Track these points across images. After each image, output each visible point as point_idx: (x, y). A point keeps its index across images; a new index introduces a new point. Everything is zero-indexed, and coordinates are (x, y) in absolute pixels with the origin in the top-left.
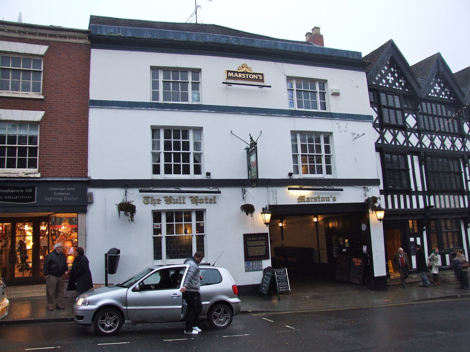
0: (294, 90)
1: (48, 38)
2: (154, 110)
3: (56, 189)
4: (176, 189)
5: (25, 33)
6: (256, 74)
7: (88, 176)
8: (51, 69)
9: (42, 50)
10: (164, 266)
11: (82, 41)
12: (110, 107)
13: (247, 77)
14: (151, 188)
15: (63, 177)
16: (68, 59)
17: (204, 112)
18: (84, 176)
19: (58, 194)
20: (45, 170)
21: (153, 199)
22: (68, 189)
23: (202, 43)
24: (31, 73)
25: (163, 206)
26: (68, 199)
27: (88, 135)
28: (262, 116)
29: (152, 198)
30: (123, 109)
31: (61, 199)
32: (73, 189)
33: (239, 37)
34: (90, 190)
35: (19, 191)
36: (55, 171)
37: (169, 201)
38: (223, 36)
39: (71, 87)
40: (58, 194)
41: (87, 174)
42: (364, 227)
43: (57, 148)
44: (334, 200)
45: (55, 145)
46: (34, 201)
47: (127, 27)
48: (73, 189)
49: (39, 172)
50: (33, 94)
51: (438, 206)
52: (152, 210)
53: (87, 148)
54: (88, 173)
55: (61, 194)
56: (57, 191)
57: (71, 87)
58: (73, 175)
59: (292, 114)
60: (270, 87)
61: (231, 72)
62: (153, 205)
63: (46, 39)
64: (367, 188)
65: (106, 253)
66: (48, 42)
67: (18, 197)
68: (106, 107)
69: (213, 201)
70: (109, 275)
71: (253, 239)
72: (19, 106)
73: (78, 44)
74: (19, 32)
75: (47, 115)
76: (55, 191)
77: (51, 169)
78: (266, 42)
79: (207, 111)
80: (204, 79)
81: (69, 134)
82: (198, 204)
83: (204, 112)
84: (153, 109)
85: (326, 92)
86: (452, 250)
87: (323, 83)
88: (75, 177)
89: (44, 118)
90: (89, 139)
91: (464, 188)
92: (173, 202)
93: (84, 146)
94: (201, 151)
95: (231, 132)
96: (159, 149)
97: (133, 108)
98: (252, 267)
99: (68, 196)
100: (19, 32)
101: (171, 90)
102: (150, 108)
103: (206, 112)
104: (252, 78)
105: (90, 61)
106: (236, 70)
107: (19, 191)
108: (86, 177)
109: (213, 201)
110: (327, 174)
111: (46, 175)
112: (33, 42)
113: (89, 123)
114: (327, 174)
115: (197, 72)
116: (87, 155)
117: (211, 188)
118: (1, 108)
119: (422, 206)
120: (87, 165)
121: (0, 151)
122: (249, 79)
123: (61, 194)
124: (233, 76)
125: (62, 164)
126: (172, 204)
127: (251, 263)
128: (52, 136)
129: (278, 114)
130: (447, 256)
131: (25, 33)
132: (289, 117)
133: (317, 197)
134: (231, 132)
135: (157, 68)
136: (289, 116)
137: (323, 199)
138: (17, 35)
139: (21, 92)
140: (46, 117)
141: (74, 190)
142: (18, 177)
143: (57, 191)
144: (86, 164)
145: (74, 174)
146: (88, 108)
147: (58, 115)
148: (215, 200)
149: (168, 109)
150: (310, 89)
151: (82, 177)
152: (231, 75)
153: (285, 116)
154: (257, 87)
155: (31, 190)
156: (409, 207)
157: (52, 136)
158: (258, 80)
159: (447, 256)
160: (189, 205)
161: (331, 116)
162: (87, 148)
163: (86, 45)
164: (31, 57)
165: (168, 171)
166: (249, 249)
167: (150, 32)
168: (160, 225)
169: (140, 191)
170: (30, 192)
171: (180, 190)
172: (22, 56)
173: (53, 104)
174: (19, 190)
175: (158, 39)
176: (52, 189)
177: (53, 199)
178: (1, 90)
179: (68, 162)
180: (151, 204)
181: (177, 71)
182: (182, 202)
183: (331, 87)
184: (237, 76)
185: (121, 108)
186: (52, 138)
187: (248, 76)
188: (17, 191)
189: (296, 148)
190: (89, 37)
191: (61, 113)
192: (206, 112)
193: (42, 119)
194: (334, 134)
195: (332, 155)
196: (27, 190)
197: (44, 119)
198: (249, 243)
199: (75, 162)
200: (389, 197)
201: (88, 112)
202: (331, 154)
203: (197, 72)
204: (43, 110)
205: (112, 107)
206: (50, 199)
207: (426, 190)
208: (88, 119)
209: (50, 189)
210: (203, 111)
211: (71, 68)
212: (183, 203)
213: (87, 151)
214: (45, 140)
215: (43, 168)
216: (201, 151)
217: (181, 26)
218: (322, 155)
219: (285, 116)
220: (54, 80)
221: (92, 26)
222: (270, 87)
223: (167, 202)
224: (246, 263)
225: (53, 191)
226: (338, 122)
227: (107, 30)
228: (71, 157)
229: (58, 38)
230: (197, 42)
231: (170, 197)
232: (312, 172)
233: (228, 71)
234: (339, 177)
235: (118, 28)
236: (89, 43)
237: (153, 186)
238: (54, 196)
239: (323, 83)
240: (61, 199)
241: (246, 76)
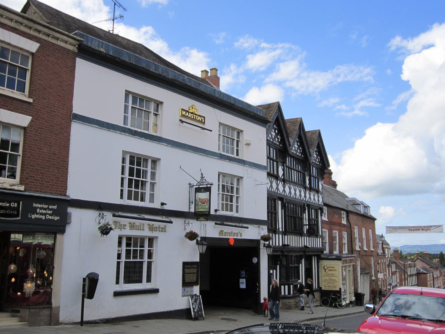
0: (151, 112)
1: (41, 36)
2: (126, 135)
3: (40, 206)
4: (139, 216)
5: (21, 24)
6: (200, 116)
7: (67, 194)
8: (40, 70)
9: (33, 46)
10: (349, 273)
11: (71, 48)
12: (90, 125)
13: (194, 118)
14: (120, 213)
15: (45, 193)
16: (56, 63)
17: (163, 144)
18: (63, 194)
19: (41, 211)
20: (28, 183)
21: (121, 224)
22: (51, 207)
23: (170, 79)
24: (17, 69)
25: (128, 232)
26: (50, 217)
27: (69, 150)
28: (113, 133)
29: (119, 222)
30: (101, 129)
31: (44, 217)
32: (55, 207)
33: (192, 79)
34: (70, 210)
35: (5, 205)
36: (37, 185)
37: (132, 226)
38: (180, 75)
39: (57, 95)
40: (41, 211)
41: (66, 192)
42: (255, 260)
43: (41, 160)
44: (241, 236)
45: (39, 156)
46: (18, 217)
47: (110, 44)
48: (55, 207)
49: (21, 183)
50: (20, 94)
51: (291, 245)
52: (119, 235)
53: (68, 164)
54: (68, 191)
55: (44, 212)
56: (41, 209)
57: (57, 95)
58: (53, 192)
59: (222, 157)
60: (211, 131)
61: (184, 110)
62: (119, 229)
63: (39, 35)
64: (103, 214)
65: (85, 277)
66: (29, 35)
67: (3, 211)
68: (87, 124)
69: (164, 230)
70: (86, 300)
71: (189, 267)
72: (7, 106)
73: (66, 50)
74: (17, 22)
75: (34, 121)
76: (38, 208)
77: (33, 182)
78: (208, 88)
79: (166, 144)
80: (164, 110)
81: (52, 146)
82: (154, 231)
83: (163, 144)
84: (126, 134)
85: (159, 114)
86: (295, 282)
87: (239, 132)
88: (55, 194)
89: (31, 124)
90: (70, 155)
91: (363, 237)
92: (135, 228)
93: (65, 162)
94: (155, 181)
95: (180, 167)
96: (146, 178)
97: (110, 129)
98: (186, 292)
99: (50, 215)
100: (17, 22)
101: (136, 117)
102: (123, 133)
103: (164, 145)
104: (198, 119)
105: (75, 70)
106: (187, 109)
107: (5, 205)
108: (65, 195)
109: (163, 230)
110: (150, 202)
111: (40, 190)
112: (26, 36)
113: (71, 137)
114: (150, 202)
115: (158, 104)
116: (67, 172)
117: (164, 217)
118: (2, 108)
119: (281, 244)
120: (67, 182)
121: (1, 158)
122: (195, 120)
123: (44, 212)
124: (185, 115)
125: (44, 179)
126: (135, 230)
127: (186, 289)
128: (37, 146)
129: (212, 156)
130: (292, 286)
131: (21, 24)
132: (218, 159)
133: (231, 232)
134: (180, 167)
135: (129, 92)
136: (218, 158)
137: (156, 228)
138: (12, 24)
139: (5, 88)
140: (32, 124)
141: (56, 208)
142: (3, 187)
143: (41, 209)
144: (66, 181)
145: (54, 191)
146: (71, 121)
147: (44, 124)
148: (165, 229)
149: (137, 137)
150: (9, 60)
151: (61, 195)
152: (184, 113)
153: (216, 158)
154: (200, 128)
155: (16, 205)
156: (316, 246)
157: (37, 146)
158: (201, 122)
159: (292, 286)
160: (146, 233)
161: (243, 162)
162: (68, 164)
163: (73, 52)
164: (20, 51)
165: (129, 198)
166: (186, 276)
167: (128, 55)
168: (120, 250)
169: (114, 216)
170: (15, 206)
171: (171, 220)
172: (12, 47)
173: (40, 110)
174: (4, 204)
175: (137, 66)
176: (36, 205)
177: (36, 216)
178: (1, 86)
179: (50, 177)
180: (119, 228)
181: (150, 101)
182: (142, 228)
183: (245, 138)
184: (188, 115)
185: (100, 127)
186: (37, 148)
187: (195, 117)
188: (3, 204)
189: (335, 210)
190: (79, 46)
191: (46, 122)
192: (164, 145)
193: (28, 125)
194: (244, 178)
195: (240, 197)
196: (13, 204)
197: (30, 126)
198: (187, 271)
199: (56, 178)
200: (310, 238)
201: (70, 126)
202: (125, 175)
203: (158, 104)
204: (30, 115)
205: (93, 125)
206: (34, 216)
207: (29, 214)
208: (70, 133)
209: (34, 205)
210: (163, 144)
211: (58, 74)
212: (143, 230)
213: (68, 167)
214: (30, 149)
215: (26, 180)
216: (155, 181)
217: (151, 56)
218: (148, 181)
219: (216, 158)
220: (42, 84)
221: (79, 33)
222: (211, 131)
223: (131, 228)
224: (183, 289)
225: (37, 208)
226: (247, 168)
227: (92, 41)
228: (53, 172)
229: (13, 23)
230: (167, 77)
231: (134, 223)
232: (136, 199)
233: (182, 110)
234: (245, 216)
235: (102, 42)
236: (76, 50)
237: (232, 221)
238: (37, 214)
239: (239, 132)
240: (43, 217)
241: (194, 116)
